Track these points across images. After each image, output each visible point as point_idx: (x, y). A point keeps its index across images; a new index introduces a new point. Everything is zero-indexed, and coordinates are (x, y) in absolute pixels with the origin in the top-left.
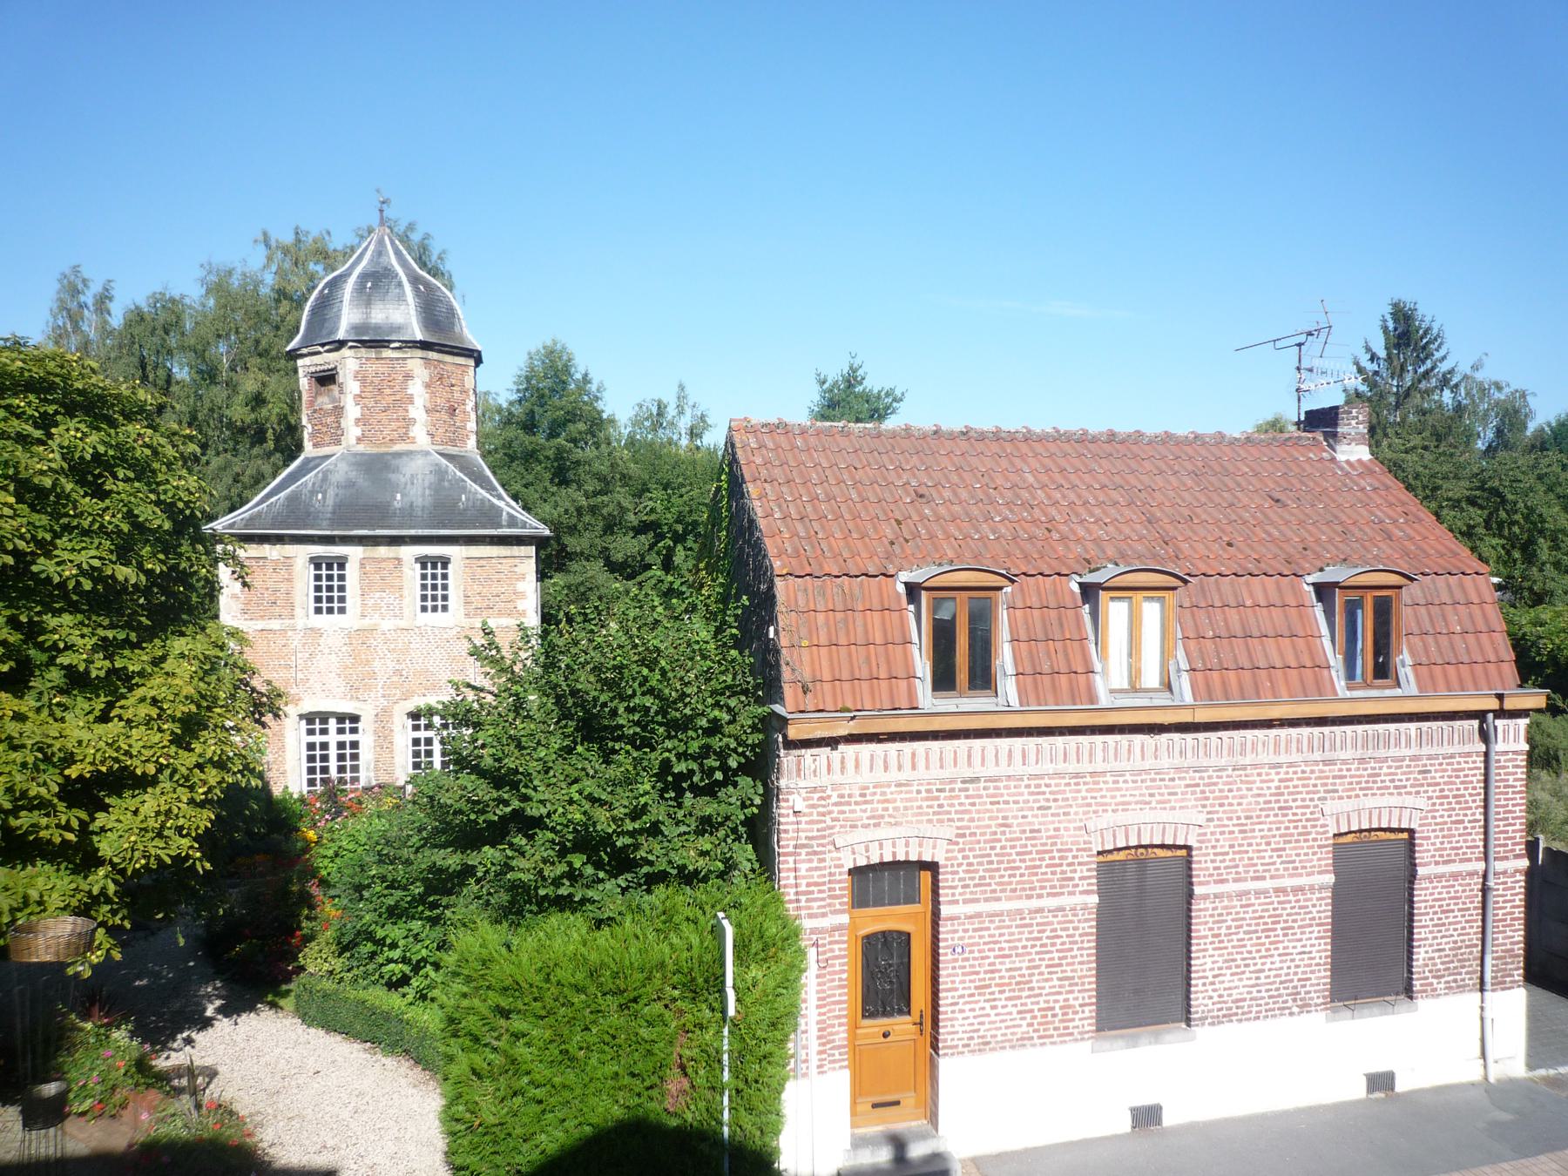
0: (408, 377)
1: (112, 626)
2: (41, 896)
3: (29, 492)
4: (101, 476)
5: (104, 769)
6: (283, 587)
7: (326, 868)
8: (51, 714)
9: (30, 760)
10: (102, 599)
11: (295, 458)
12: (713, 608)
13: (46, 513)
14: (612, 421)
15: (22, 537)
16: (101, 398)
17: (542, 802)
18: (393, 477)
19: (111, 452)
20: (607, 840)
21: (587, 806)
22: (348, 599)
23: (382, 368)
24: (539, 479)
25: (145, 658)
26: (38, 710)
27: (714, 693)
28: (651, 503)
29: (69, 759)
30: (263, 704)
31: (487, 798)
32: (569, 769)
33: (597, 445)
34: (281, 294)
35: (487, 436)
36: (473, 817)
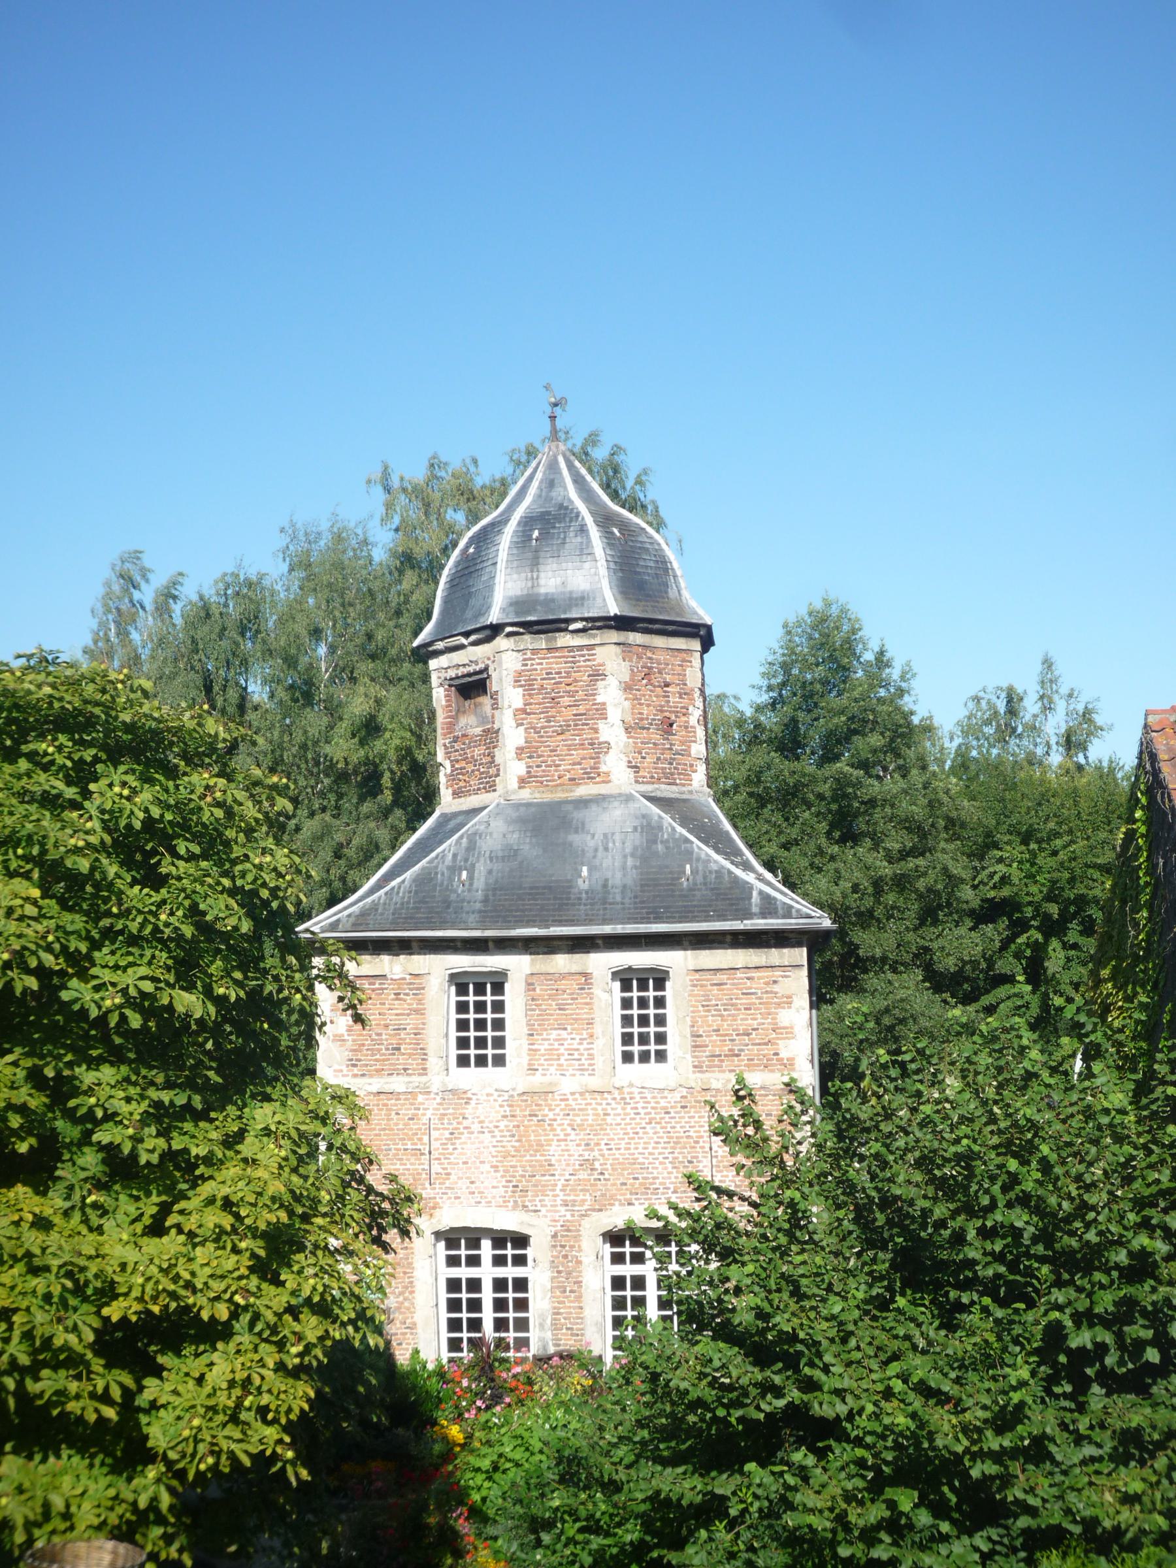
0: (597, 675)
1: (169, 1085)
2: (68, 1506)
3: (63, 883)
4: (154, 852)
5: (156, 1309)
6: (411, 1022)
7: (480, 1488)
8: (85, 1221)
9: (56, 1290)
10: (156, 1043)
11: (424, 817)
12: (1130, 1049)
13: (81, 911)
14: (928, 729)
15: (49, 949)
16: (155, 733)
17: (839, 1393)
18: (575, 839)
19: (169, 817)
20: (953, 1465)
21: (917, 1403)
22: (508, 1042)
23: (555, 664)
24: (808, 833)
25: (214, 1135)
26: (67, 1214)
27: (1140, 1204)
28: (1001, 869)
29: (109, 1292)
30: (383, 1213)
31: (744, 1381)
32: (882, 1338)
33: (904, 771)
34: (407, 560)
35: (721, 765)
36: (721, 1412)
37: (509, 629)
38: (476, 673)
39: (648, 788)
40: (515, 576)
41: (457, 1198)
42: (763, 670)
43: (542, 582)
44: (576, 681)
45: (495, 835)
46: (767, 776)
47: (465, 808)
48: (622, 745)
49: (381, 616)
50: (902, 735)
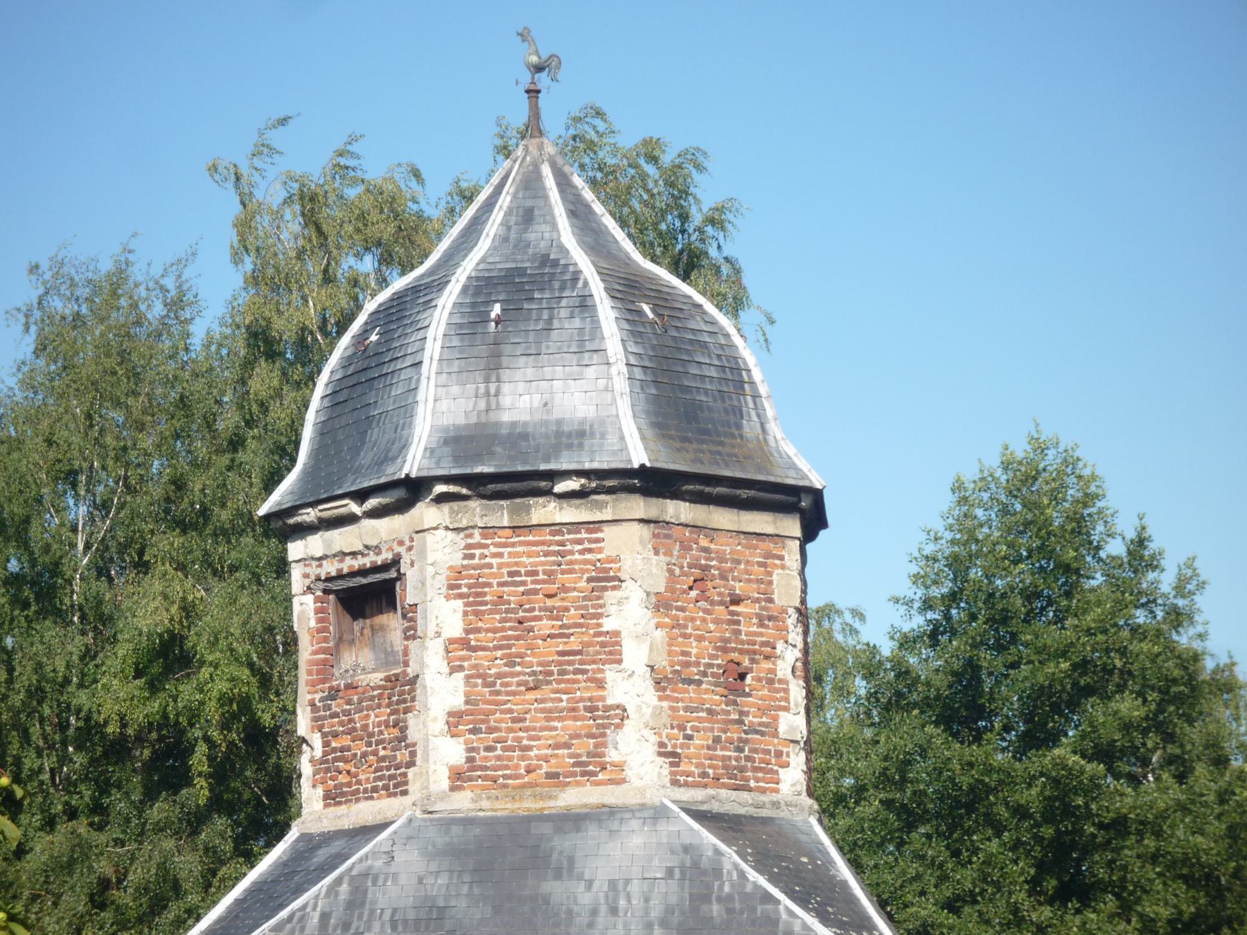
0: (606, 579)
18: (555, 889)
23: (526, 555)
34: (262, 342)
37: (440, 488)
39: (696, 795)
40: (455, 389)
42: (914, 569)
43: (506, 401)
44: (564, 589)
45: (403, 879)
46: (920, 771)
47: (346, 824)
48: (648, 711)
49: (201, 449)
50: (1178, 699)
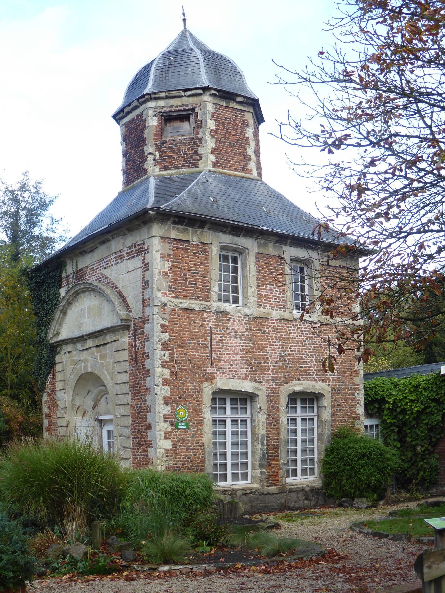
23: (229, 114)
38: (185, 110)
41: (224, 373)
